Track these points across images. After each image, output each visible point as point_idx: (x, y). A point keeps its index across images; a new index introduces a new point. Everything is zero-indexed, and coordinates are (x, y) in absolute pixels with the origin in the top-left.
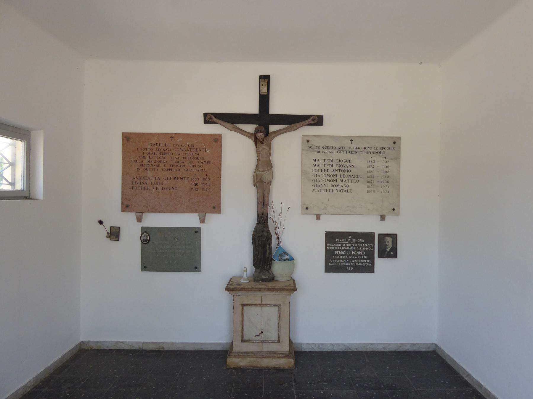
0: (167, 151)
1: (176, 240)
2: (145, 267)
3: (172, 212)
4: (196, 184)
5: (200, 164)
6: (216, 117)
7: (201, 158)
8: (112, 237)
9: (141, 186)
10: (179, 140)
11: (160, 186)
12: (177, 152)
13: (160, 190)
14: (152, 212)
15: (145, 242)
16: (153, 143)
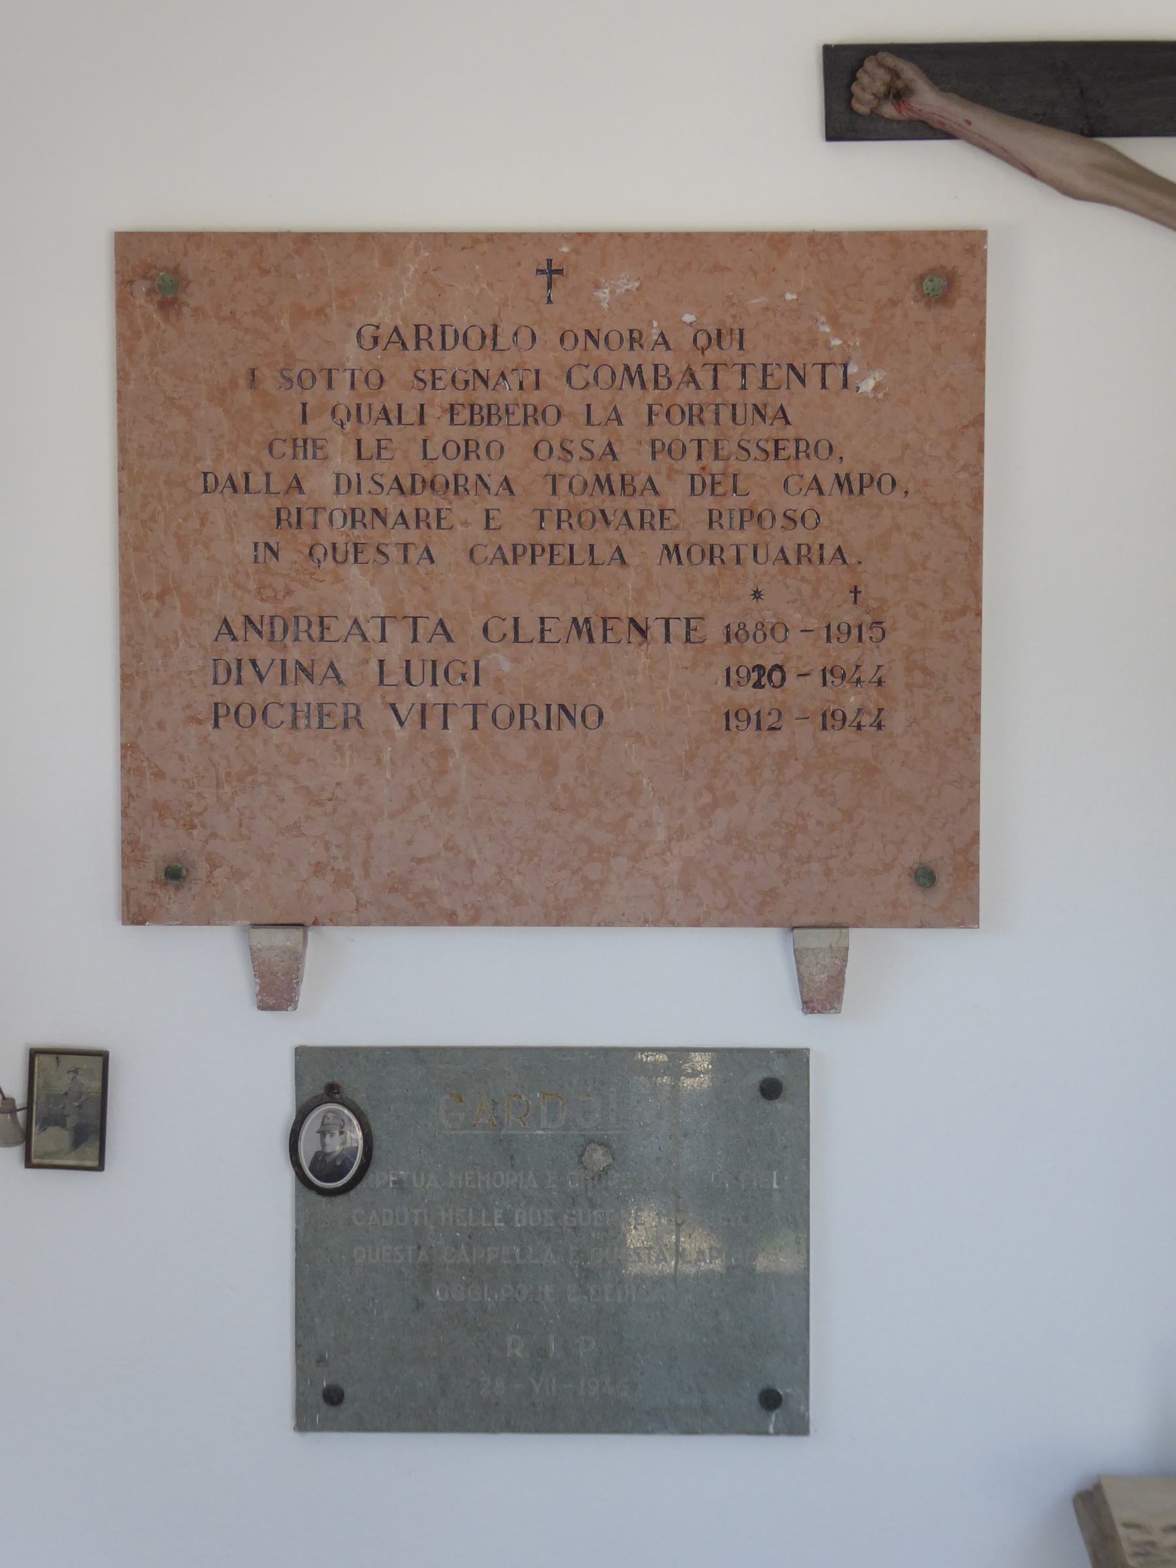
0: (507, 394)
1: (599, 1157)
2: (334, 1397)
3: (559, 915)
4: (763, 675)
5: (803, 503)
6: (939, 81)
7: (804, 449)
8: (46, 1139)
9: (286, 694)
10: (610, 294)
11: (460, 695)
12: (600, 399)
13: (456, 734)
14: (391, 918)
15: (323, 1180)
16: (386, 318)
